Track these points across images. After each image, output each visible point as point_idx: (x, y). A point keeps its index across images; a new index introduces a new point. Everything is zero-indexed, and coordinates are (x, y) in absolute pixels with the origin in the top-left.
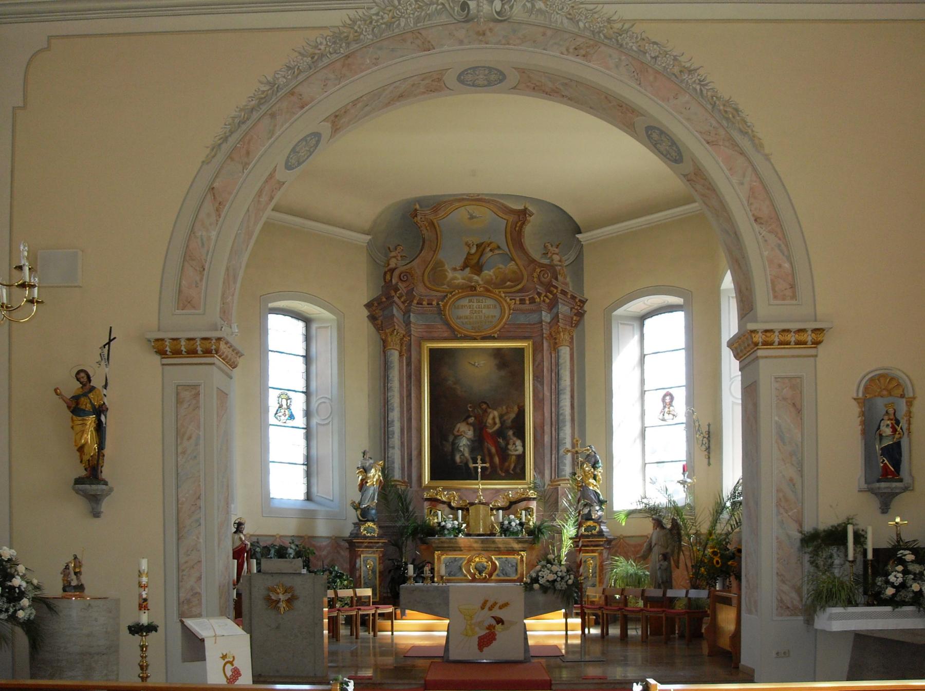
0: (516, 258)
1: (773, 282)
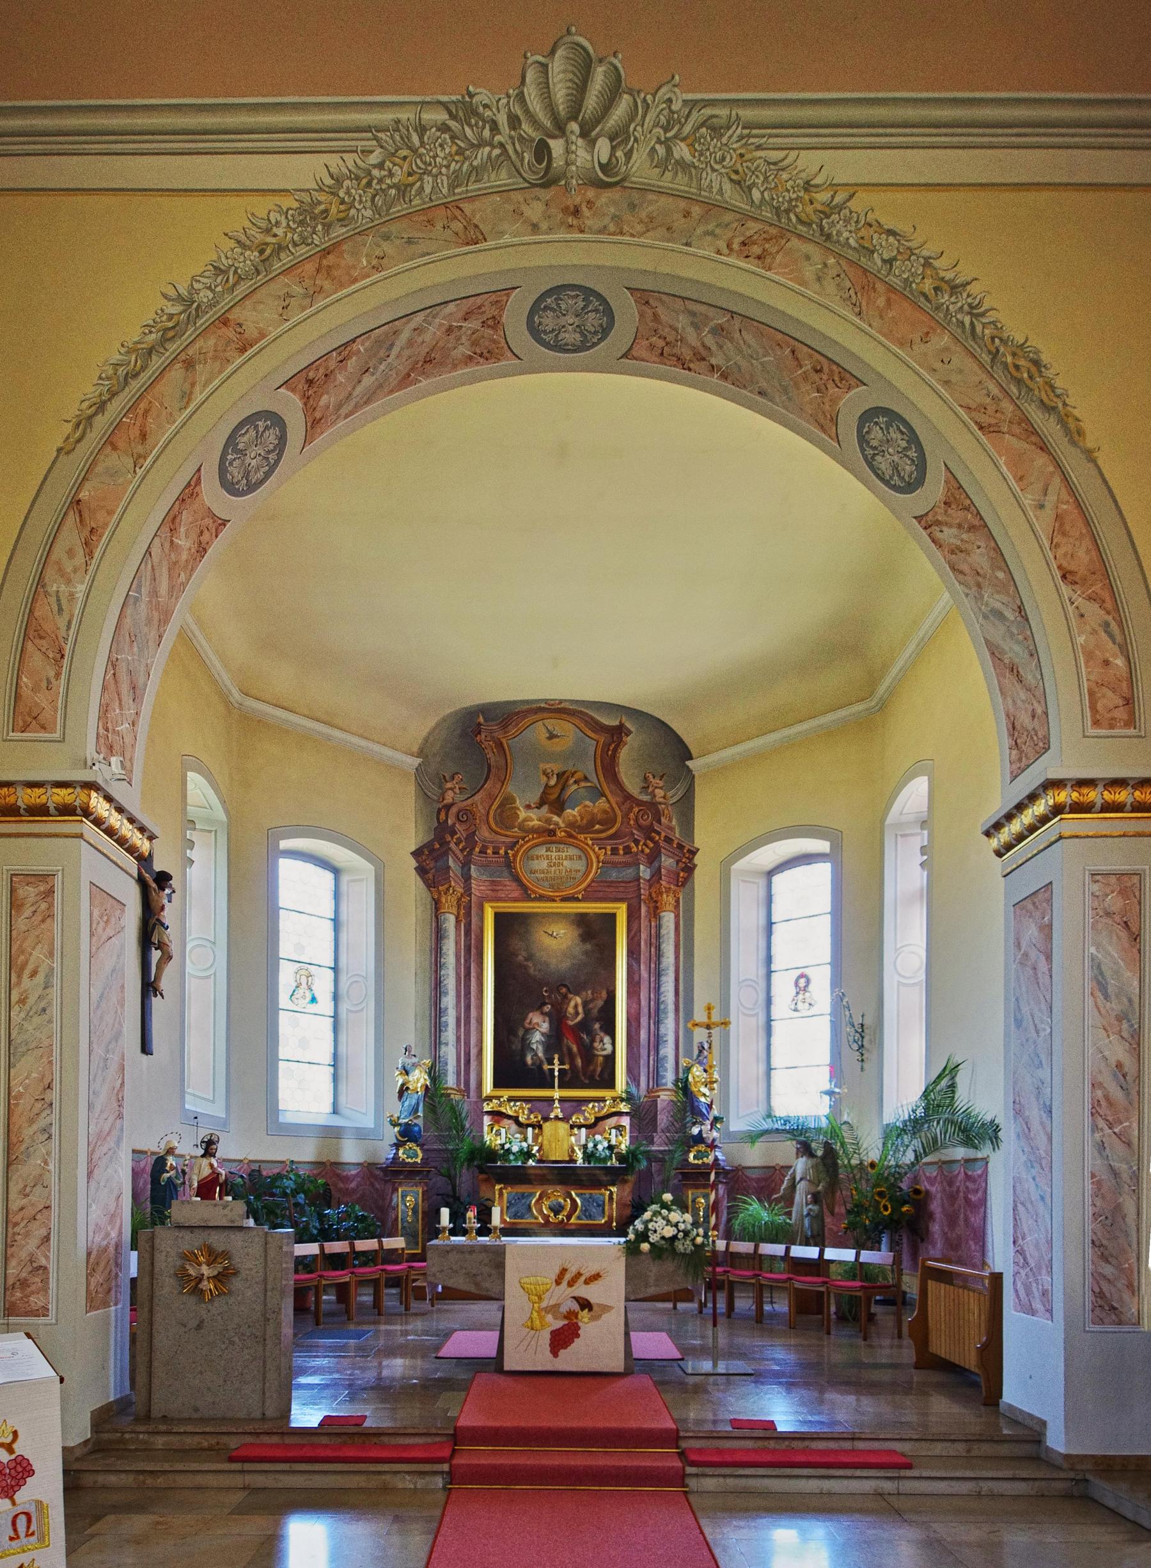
0: (608, 793)
1: (1091, 694)
